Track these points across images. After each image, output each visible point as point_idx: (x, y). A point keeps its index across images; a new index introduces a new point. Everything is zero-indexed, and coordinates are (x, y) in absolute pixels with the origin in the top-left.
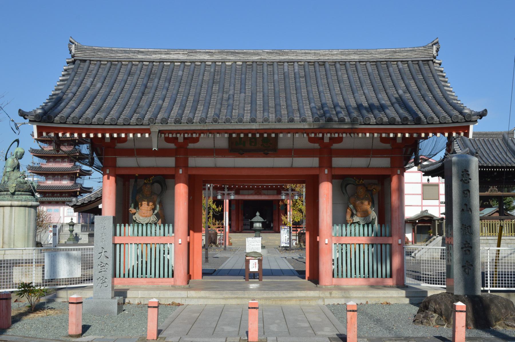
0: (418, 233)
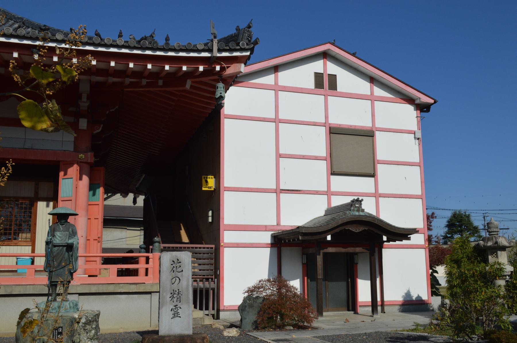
0: (326, 278)
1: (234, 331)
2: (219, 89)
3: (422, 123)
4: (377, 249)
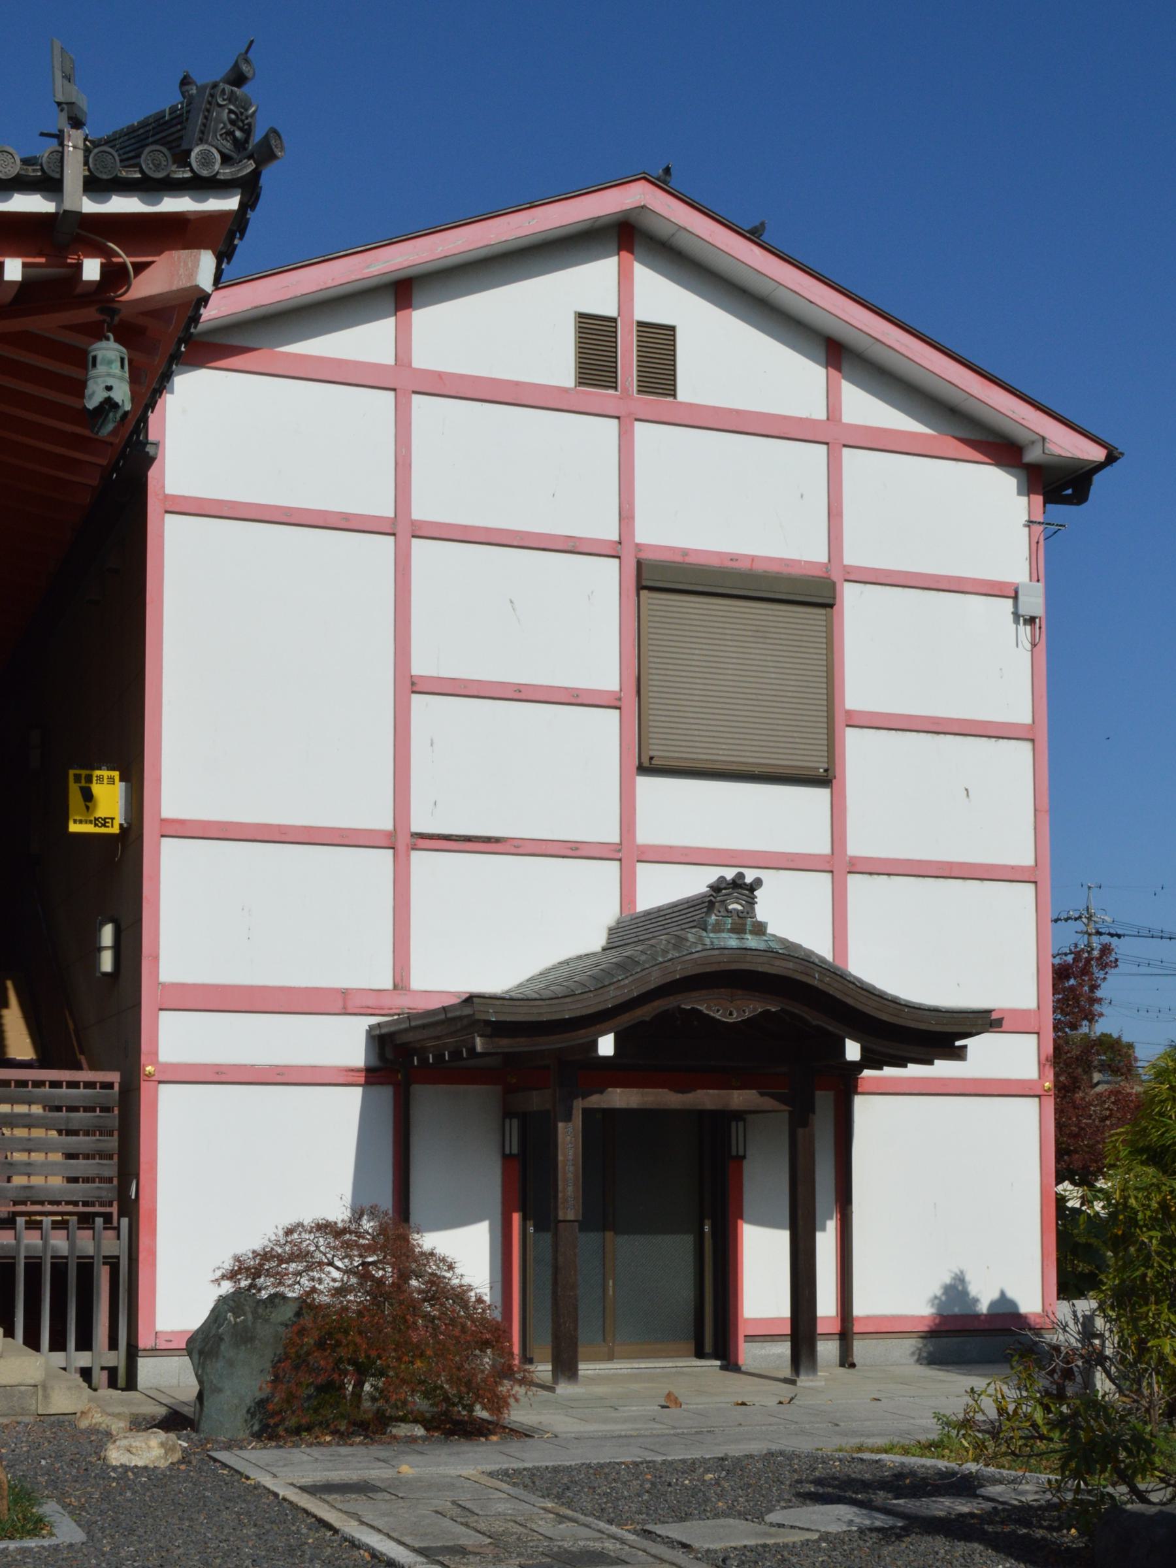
0: (602, 1215)
1: (154, 1443)
2: (101, 369)
3: (1051, 551)
4: (824, 1101)
